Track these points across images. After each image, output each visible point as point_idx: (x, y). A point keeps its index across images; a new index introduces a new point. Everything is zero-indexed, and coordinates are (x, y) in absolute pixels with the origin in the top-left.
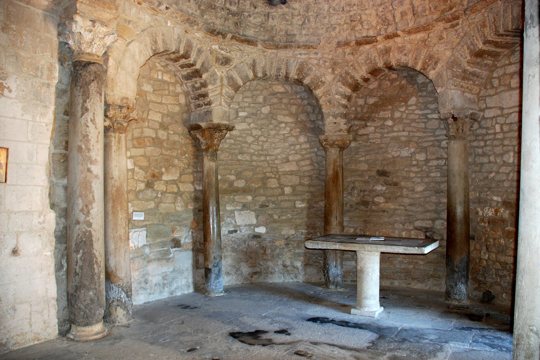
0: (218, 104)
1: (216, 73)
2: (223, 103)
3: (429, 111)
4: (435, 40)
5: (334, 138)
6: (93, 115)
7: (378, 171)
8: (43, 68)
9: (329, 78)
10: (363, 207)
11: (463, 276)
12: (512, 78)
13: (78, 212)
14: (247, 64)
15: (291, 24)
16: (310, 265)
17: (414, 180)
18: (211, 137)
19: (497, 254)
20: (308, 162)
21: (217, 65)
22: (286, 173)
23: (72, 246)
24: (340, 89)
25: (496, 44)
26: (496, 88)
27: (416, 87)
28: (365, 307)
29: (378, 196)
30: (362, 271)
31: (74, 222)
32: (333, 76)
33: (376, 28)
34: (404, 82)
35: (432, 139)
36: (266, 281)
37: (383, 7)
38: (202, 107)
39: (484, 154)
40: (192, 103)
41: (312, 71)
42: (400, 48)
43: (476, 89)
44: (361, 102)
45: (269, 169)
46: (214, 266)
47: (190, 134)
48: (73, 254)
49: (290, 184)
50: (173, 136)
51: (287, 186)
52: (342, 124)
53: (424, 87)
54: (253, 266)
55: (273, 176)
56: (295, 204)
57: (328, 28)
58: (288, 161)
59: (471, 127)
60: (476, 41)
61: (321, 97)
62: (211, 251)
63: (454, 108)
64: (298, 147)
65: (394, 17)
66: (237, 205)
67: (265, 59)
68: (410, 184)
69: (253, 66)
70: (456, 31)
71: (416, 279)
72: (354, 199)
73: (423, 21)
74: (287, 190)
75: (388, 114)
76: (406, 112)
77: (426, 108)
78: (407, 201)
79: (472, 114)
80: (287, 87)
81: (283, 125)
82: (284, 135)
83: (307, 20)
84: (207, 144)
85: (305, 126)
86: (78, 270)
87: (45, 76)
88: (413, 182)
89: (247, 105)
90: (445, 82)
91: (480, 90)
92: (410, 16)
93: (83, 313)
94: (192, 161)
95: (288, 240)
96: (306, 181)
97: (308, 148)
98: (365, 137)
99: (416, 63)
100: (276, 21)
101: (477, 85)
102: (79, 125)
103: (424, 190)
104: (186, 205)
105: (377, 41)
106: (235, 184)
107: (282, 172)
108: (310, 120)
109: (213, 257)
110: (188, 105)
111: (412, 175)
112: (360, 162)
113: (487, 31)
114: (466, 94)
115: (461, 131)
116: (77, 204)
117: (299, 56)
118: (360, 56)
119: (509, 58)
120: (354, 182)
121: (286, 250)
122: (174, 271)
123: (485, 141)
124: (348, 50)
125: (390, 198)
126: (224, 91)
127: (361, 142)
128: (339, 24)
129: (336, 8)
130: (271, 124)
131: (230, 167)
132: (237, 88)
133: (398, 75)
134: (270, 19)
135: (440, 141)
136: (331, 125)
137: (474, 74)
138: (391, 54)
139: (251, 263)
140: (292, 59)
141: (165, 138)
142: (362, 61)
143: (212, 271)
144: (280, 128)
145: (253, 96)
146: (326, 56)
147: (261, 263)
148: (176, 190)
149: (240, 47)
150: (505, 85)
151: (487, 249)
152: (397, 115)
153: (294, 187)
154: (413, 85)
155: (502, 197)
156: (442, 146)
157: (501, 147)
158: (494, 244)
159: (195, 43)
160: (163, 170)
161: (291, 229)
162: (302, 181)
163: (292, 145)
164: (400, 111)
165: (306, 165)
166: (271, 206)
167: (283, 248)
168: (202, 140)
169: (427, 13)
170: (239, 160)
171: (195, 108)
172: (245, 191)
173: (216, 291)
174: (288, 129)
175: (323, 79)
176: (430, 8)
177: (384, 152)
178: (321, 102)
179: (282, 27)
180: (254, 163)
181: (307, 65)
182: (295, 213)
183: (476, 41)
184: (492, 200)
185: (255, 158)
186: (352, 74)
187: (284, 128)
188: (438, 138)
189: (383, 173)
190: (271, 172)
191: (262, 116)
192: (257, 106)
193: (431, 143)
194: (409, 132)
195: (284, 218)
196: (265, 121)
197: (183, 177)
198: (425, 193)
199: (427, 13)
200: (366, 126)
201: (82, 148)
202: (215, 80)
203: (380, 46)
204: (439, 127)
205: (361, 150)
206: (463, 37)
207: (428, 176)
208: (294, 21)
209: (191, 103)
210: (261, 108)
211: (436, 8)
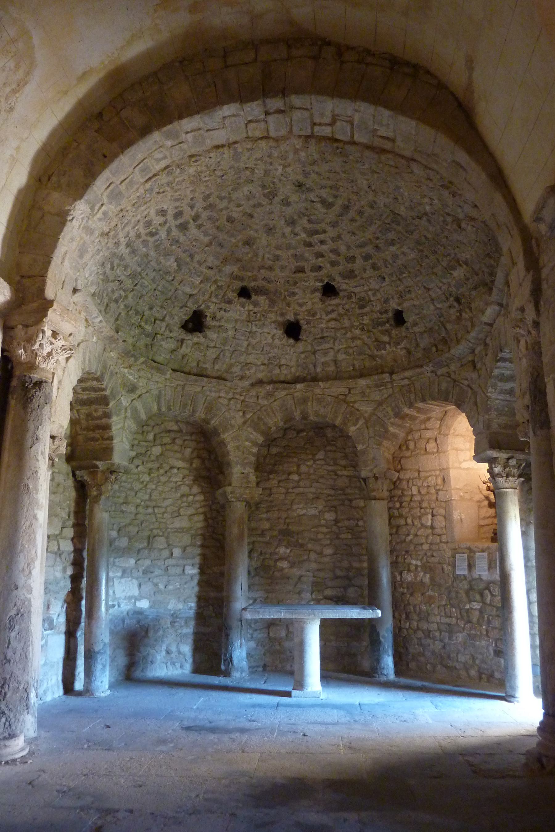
1: (121, 403)
2: (124, 439)
6: (43, 447)
9: (238, 419)
20: (201, 517)
21: (123, 393)
24: (251, 436)
27: (325, 440)
29: (281, 559)
39: (401, 516)
40: (80, 435)
47: (74, 475)
49: (180, 544)
53: (333, 441)
61: (229, 442)
64: (191, 498)
74: (177, 552)
78: (314, 566)
81: (175, 471)
83: (222, 353)
88: (321, 545)
94: (72, 509)
95: (175, 616)
104: (64, 570)
107: (171, 529)
111: (320, 536)
117: (208, 393)
126: (126, 424)
128: (256, 365)
130: (162, 468)
138: (309, 404)
140: (201, 395)
146: (238, 396)
152: (303, 469)
155: (421, 560)
164: (307, 465)
174: (182, 476)
188: (350, 497)
191: (153, 458)
196: (156, 465)
197: (65, 530)
200: (269, 479)
205: (262, 506)
207: (338, 538)
210: (151, 447)
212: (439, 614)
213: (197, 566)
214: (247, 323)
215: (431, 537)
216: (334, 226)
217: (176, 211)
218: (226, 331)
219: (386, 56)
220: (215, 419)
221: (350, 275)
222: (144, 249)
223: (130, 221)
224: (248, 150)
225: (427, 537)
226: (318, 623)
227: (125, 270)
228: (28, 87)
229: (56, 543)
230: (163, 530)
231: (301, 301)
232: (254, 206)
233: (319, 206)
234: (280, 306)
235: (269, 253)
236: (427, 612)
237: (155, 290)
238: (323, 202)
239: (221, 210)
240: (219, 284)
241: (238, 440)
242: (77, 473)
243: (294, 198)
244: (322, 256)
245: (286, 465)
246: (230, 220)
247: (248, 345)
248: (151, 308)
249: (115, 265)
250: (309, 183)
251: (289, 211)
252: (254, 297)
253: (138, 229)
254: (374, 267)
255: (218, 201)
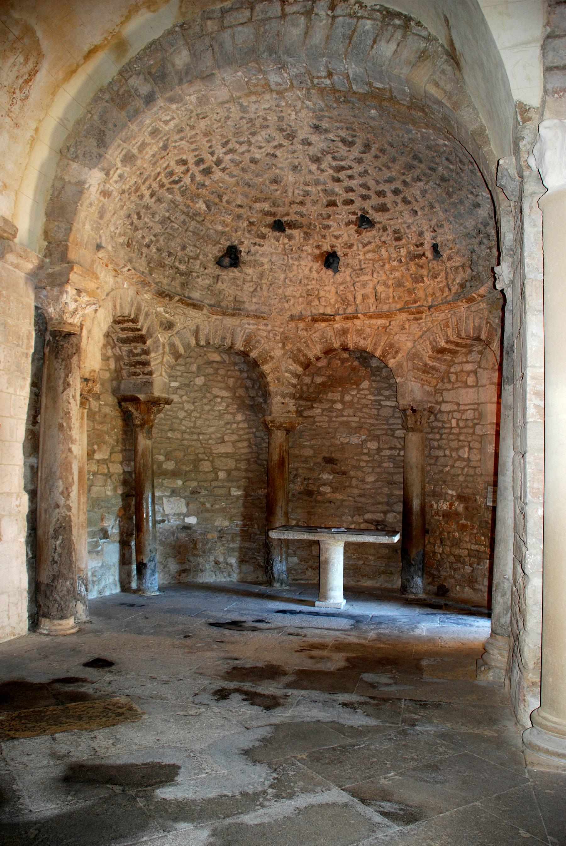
0: (159, 374)
2: (164, 373)
3: (383, 398)
4: (396, 329)
5: (282, 420)
7: (324, 458)
8: (23, 336)
9: (278, 353)
10: (306, 498)
11: (419, 569)
12: (468, 376)
13: (58, 495)
14: (190, 330)
15: (241, 290)
16: (246, 562)
17: (364, 469)
18: (149, 411)
19: (451, 547)
20: (245, 444)
21: (160, 330)
22: (221, 455)
23: (49, 532)
24: (291, 367)
25: (457, 344)
26: (453, 383)
27: (369, 370)
28: (331, 599)
29: (324, 485)
30: (327, 562)
31: (53, 506)
32: (283, 351)
33: (334, 306)
34: (356, 363)
35: (386, 427)
36: (195, 580)
37: (344, 286)
38: (138, 375)
39: (439, 448)
41: (260, 343)
42: (358, 331)
43: (434, 382)
44: (307, 380)
45: (202, 450)
46: (150, 561)
47: (120, 405)
48: (50, 541)
50: (104, 407)
51: (222, 470)
52: (291, 405)
53: (378, 371)
54: (182, 563)
55: (206, 458)
56: (229, 491)
57: (282, 298)
58: (223, 442)
59: (428, 419)
60: (438, 339)
61: (269, 374)
62: (147, 543)
63: (413, 400)
64: (235, 426)
65: (355, 298)
66: (165, 490)
67: (209, 326)
68: (360, 474)
69: (196, 333)
70: (419, 324)
71: (365, 575)
72: (297, 487)
73: (385, 308)
74: (222, 475)
75: (337, 396)
76: (358, 396)
77: (380, 394)
78: (356, 492)
79: (430, 408)
80: (224, 356)
81: (219, 400)
82: (219, 411)
84: (143, 419)
85: (244, 402)
86: (56, 558)
87: (24, 346)
88: (363, 472)
89: (179, 374)
90: (405, 373)
91: (438, 382)
92: (372, 300)
93: (57, 605)
94: (120, 437)
95: (222, 533)
96: (243, 466)
97: (246, 428)
98: (311, 419)
99: (376, 349)
100: (225, 285)
101: (436, 378)
102: (61, 401)
103: (376, 481)
104: (115, 489)
105: (335, 320)
106: (164, 466)
108: (250, 396)
109: (148, 549)
110: (118, 371)
111: (362, 464)
112: (305, 447)
113: (450, 331)
114: (425, 387)
115: (419, 423)
116: (57, 487)
117: (247, 326)
118: (314, 333)
119: (466, 357)
120: (297, 469)
121: (219, 544)
122: (102, 566)
123: (441, 435)
124: (301, 325)
125: (337, 488)
126: (165, 360)
127: (305, 425)
128: (294, 297)
129: (294, 279)
130: (205, 397)
131: (159, 446)
132: (177, 356)
133: (350, 355)
134: (220, 283)
135: (393, 430)
136: (279, 405)
137: (433, 368)
138: (349, 336)
139: (179, 559)
140: (239, 329)
141: (97, 410)
142: (317, 339)
143: (148, 566)
144: (216, 403)
145: (186, 364)
146: (277, 329)
147: (191, 559)
148: (106, 471)
149: (184, 310)
150: (461, 382)
151: (441, 542)
152: (347, 398)
153: (229, 472)
154: (366, 367)
156: (396, 435)
157: (456, 441)
158: (449, 538)
159: (143, 304)
160: (96, 447)
161: (225, 520)
162: (238, 465)
163: (228, 423)
165: (243, 448)
166: (204, 492)
167: (216, 542)
168: (136, 413)
169: (391, 301)
170: (169, 438)
171: (129, 376)
172: (175, 474)
173: (152, 590)
174: (224, 404)
175: (272, 354)
176: (394, 297)
177: (332, 438)
178: (269, 379)
179: (231, 292)
180: (185, 442)
181: (255, 337)
182: (229, 502)
183: (438, 339)
184: (446, 493)
185: (186, 436)
186: (305, 352)
187: (220, 403)
188: (392, 427)
189: (330, 461)
190: (204, 453)
192: (189, 375)
193: (384, 432)
194: (360, 418)
195: (217, 506)
196: (198, 394)
197: (113, 455)
198: (376, 483)
199: (391, 301)
200: (313, 407)
201: (63, 426)
202: (158, 347)
203: (337, 326)
204: (394, 415)
205: (306, 434)
206: (426, 332)
207: (379, 466)
208: (245, 287)
209: (122, 369)
210: (194, 378)
211: (400, 298)
212: (470, 541)
213: (242, 488)
214: (282, 256)
215: (466, 469)
216: (359, 163)
217: (196, 159)
218: (262, 264)
219: (378, 7)
220: (254, 351)
221: (383, 208)
222: (170, 196)
223: (150, 175)
224: (255, 102)
225: (463, 469)
226: (342, 545)
227: (153, 217)
228: (39, 75)
229: (105, 466)
230: (208, 455)
231: (335, 233)
232: (275, 147)
233: (340, 144)
234: (316, 238)
235: (298, 188)
236: (460, 539)
237: (186, 231)
238: (343, 141)
239: (243, 153)
240: (251, 220)
241: (278, 372)
242: (123, 404)
243: (314, 138)
244: (352, 190)
245: (330, 394)
246: (254, 161)
247: (286, 278)
248: (184, 248)
249: (142, 214)
250: (325, 124)
251: (312, 151)
252: (288, 231)
253: (160, 180)
254: (405, 201)
255: (237, 146)
